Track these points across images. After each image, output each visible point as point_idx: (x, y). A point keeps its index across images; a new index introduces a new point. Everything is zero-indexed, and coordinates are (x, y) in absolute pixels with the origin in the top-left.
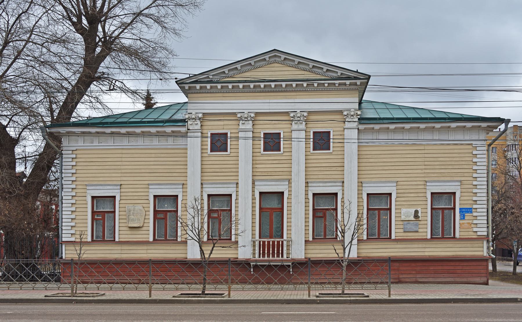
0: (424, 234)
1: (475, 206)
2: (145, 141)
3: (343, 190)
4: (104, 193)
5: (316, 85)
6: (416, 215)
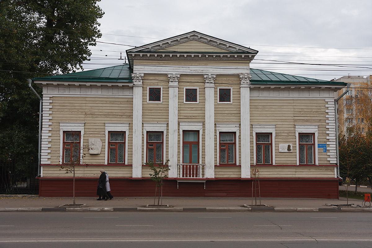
0: (103, 161)
1: (328, 143)
2: (70, 92)
3: (240, 130)
4: (77, 129)
5: (207, 56)
6: (289, 148)
